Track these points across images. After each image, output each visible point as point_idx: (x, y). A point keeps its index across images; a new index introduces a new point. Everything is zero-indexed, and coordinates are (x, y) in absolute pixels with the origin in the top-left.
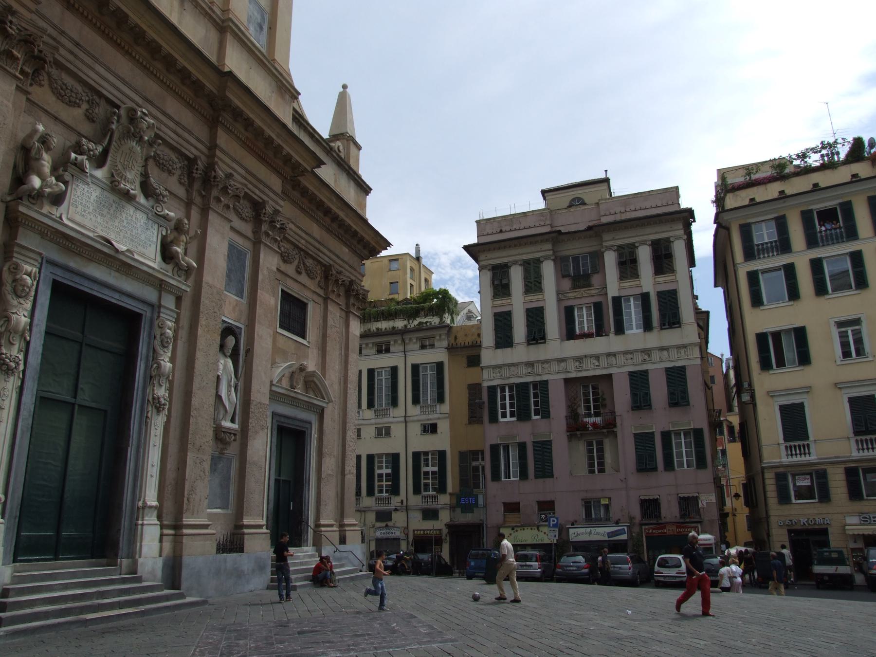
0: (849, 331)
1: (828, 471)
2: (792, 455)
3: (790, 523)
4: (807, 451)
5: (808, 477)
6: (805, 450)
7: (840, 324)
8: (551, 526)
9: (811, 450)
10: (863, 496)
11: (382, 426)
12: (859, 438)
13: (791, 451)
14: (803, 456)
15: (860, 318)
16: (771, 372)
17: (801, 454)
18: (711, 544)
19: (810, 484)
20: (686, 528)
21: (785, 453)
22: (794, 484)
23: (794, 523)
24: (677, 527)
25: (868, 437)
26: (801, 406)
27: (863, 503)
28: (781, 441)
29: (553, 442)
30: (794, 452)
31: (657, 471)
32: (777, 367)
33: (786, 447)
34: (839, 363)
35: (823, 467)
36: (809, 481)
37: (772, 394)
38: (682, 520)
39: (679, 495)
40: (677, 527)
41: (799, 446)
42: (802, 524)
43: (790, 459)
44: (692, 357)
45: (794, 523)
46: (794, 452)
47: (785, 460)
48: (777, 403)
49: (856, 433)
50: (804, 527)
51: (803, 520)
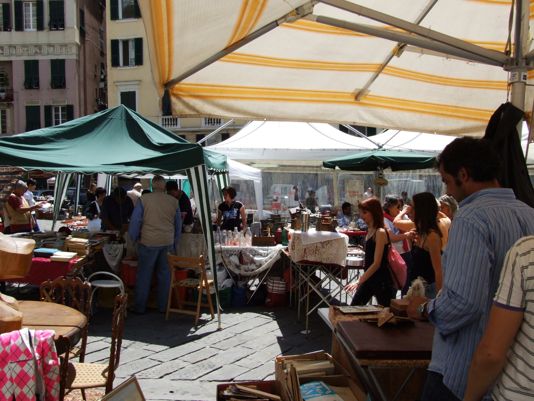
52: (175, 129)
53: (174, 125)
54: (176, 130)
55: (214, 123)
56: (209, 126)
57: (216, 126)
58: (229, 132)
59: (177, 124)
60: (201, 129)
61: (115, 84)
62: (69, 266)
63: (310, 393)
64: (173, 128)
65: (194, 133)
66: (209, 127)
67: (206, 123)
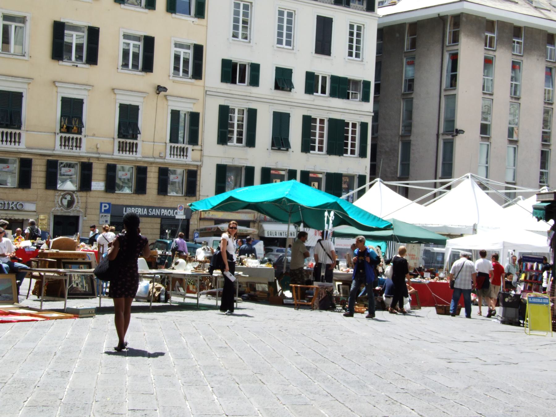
1: (34, 162)
6: (78, 144)
8: (103, 211)
52: (18, 149)
53: (15, 142)
54: (19, 150)
55: (72, 146)
56: (76, 151)
57: (129, 155)
58: (91, 161)
59: (19, 142)
60: (54, 152)
61: (55, 85)
62: (108, 290)
63: (429, 192)
64: (15, 147)
65: (43, 157)
66: (65, 152)
67: (61, 145)
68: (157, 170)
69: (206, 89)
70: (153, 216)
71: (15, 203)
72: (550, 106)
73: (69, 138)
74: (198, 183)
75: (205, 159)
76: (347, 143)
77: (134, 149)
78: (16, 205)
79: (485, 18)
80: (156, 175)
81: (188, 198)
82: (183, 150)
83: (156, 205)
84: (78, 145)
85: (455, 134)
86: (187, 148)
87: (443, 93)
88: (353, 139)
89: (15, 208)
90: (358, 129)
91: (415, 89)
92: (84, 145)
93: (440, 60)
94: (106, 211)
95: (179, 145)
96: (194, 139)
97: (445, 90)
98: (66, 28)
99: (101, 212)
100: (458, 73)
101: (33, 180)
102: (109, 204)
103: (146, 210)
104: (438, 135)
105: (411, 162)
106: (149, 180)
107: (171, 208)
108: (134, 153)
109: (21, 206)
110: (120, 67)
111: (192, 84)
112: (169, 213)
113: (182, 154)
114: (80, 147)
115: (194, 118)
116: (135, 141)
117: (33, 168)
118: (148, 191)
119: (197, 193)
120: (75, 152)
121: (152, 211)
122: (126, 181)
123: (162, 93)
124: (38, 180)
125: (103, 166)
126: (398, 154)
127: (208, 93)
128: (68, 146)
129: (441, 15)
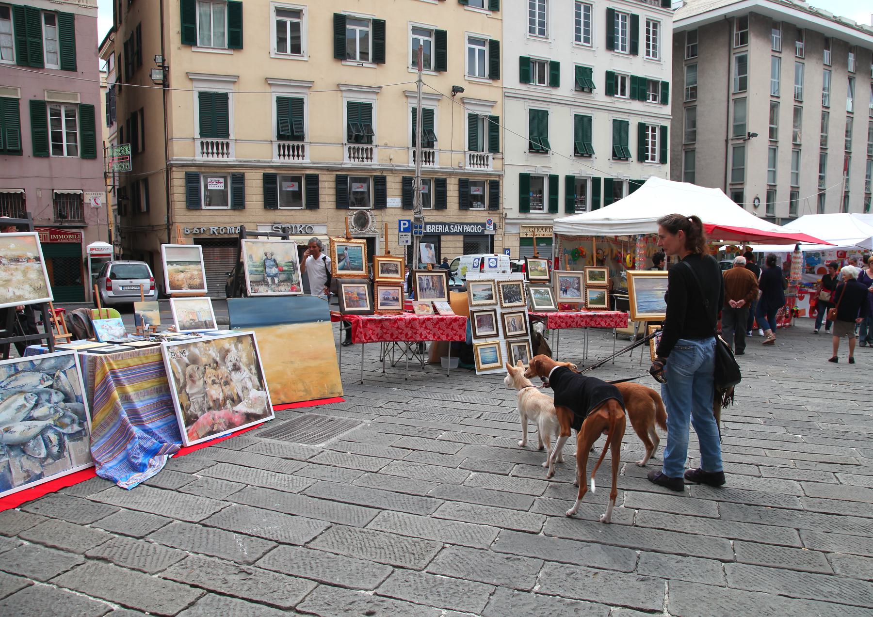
0: (289, 21)
1: (321, 178)
2: (208, 153)
3: (198, 232)
4: (300, 153)
5: (222, 180)
6: (298, 151)
7: (280, 11)
8: (402, 230)
9: (230, 150)
10: (201, 206)
11: (291, 58)
12: (282, 143)
13: (207, 149)
14: (220, 155)
15: (302, 10)
16: (194, 49)
17: (218, 154)
18: (109, 255)
19: (297, 189)
20: (64, 234)
21: (201, 150)
22: (206, 186)
23: (202, 232)
24: (51, 233)
25: (291, 143)
26: (225, 97)
27: (277, 212)
28: (197, 136)
29: (20, 102)
30: (210, 151)
31: (22, 155)
32: (292, 52)
33: (202, 143)
34: (273, 56)
35: (242, 171)
36: (223, 184)
37: (191, 77)
38: (58, 224)
39: (55, 191)
40: (51, 233)
41: (217, 144)
42: (212, 232)
43: (472, 168)
44: (85, 4)
45: (202, 232)
46: (210, 151)
47: (200, 159)
48: (410, 105)
49: (280, 137)
50: (214, 237)
51: (213, 229)
59: (303, 156)
68: (457, 182)
69: (505, 90)
70: (455, 234)
71: (303, 226)
72: (827, 110)
73: (358, 149)
74: (501, 195)
75: (507, 168)
76: (648, 148)
77: (431, 159)
78: (305, 228)
79: (771, 18)
80: (456, 187)
81: (491, 212)
82: (482, 158)
83: (457, 221)
84: (369, 156)
85: (747, 137)
86: (488, 156)
87: (731, 97)
88: (653, 144)
89: (303, 232)
90: (658, 133)
91: (698, 96)
92: (375, 156)
93: (727, 64)
94: (405, 230)
95: (479, 153)
96: (494, 147)
97: (734, 94)
98: (347, 21)
99: (400, 230)
100: (748, 75)
101: (321, 198)
102: (409, 221)
103: (447, 226)
104: (727, 141)
105: (696, 170)
106: (449, 193)
107: (474, 224)
108: (431, 163)
109: (310, 230)
110: (410, 67)
111: (489, 85)
112: (472, 229)
113: (482, 162)
114: (371, 159)
115: (494, 123)
116: (431, 150)
117: (321, 185)
118: (448, 205)
119: (501, 206)
120: (366, 163)
121: (454, 228)
122: (430, 267)
123: (459, 95)
124: (327, 198)
125: (399, 179)
126: (681, 163)
127: (506, 94)
128: (358, 158)
129: (727, 17)
